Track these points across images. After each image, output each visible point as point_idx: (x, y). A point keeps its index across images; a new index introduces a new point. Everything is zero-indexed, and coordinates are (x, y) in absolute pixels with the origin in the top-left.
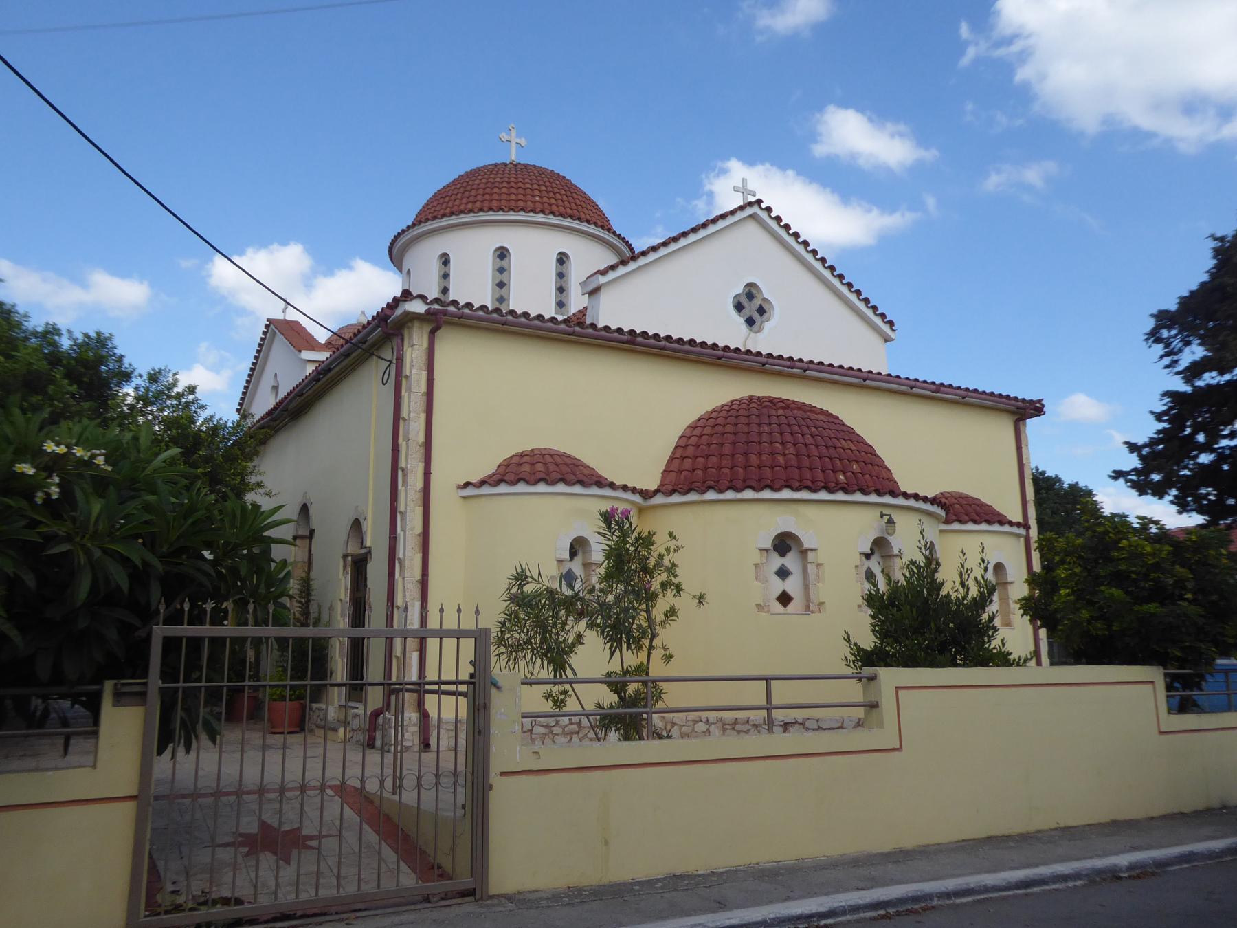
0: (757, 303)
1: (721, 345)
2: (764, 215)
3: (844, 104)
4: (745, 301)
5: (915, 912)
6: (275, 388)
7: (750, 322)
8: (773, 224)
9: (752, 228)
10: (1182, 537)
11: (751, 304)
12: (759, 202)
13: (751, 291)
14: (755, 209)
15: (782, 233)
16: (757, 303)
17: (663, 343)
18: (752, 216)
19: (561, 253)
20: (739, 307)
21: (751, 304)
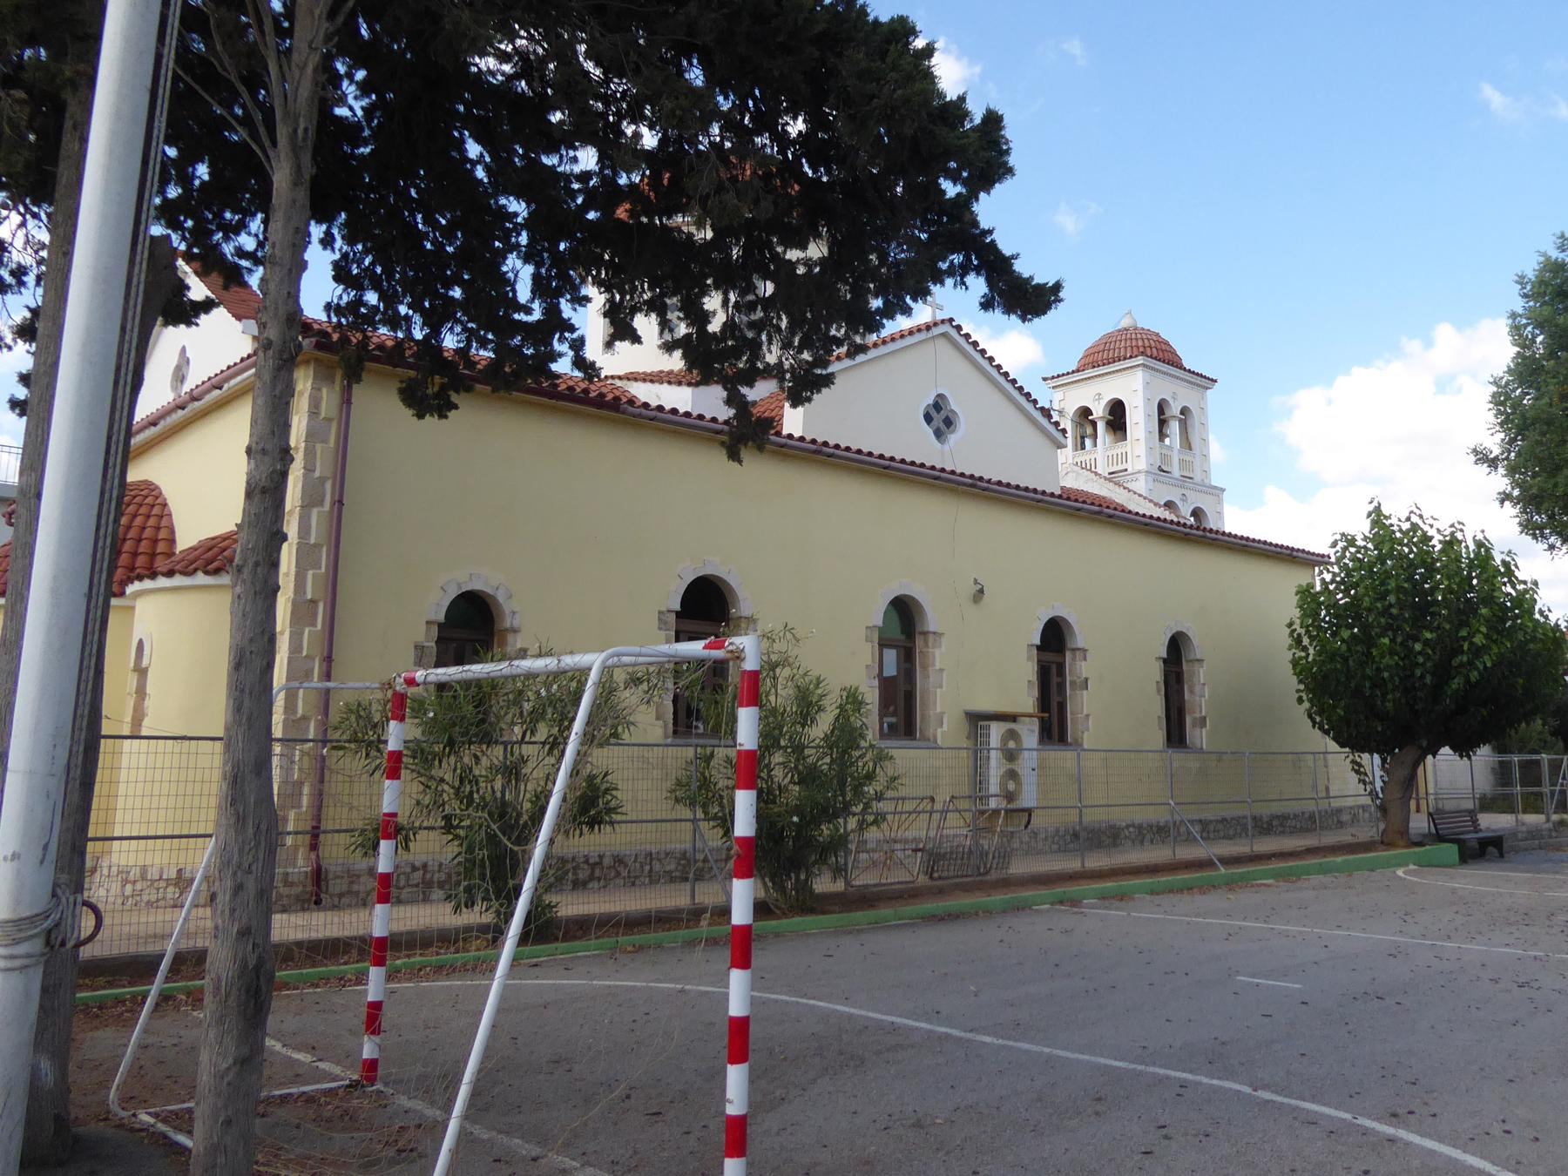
0: (943, 414)
1: (843, 446)
2: (953, 333)
3: (942, 95)
4: (933, 413)
5: (1210, 829)
6: (179, 376)
7: (939, 434)
8: (962, 341)
9: (942, 344)
10: (967, 217)
11: (940, 417)
12: (951, 320)
13: (939, 404)
14: (946, 328)
15: (978, 357)
16: (943, 414)
17: (654, 413)
18: (944, 335)
19: (940, 396)
20: (928, 418)
21: (940, 417)
